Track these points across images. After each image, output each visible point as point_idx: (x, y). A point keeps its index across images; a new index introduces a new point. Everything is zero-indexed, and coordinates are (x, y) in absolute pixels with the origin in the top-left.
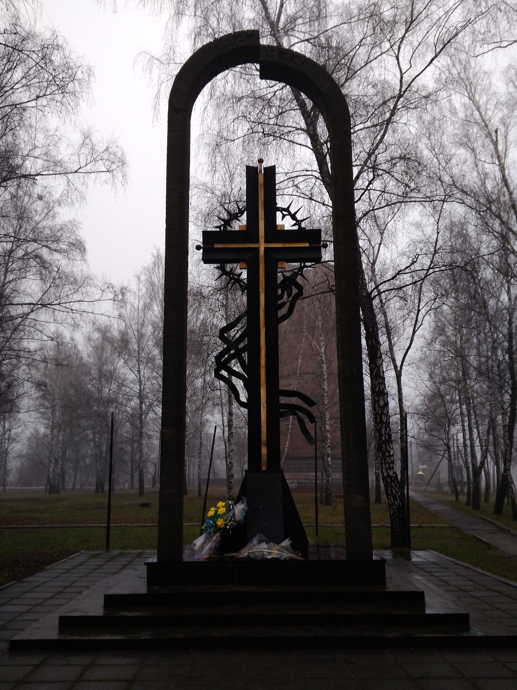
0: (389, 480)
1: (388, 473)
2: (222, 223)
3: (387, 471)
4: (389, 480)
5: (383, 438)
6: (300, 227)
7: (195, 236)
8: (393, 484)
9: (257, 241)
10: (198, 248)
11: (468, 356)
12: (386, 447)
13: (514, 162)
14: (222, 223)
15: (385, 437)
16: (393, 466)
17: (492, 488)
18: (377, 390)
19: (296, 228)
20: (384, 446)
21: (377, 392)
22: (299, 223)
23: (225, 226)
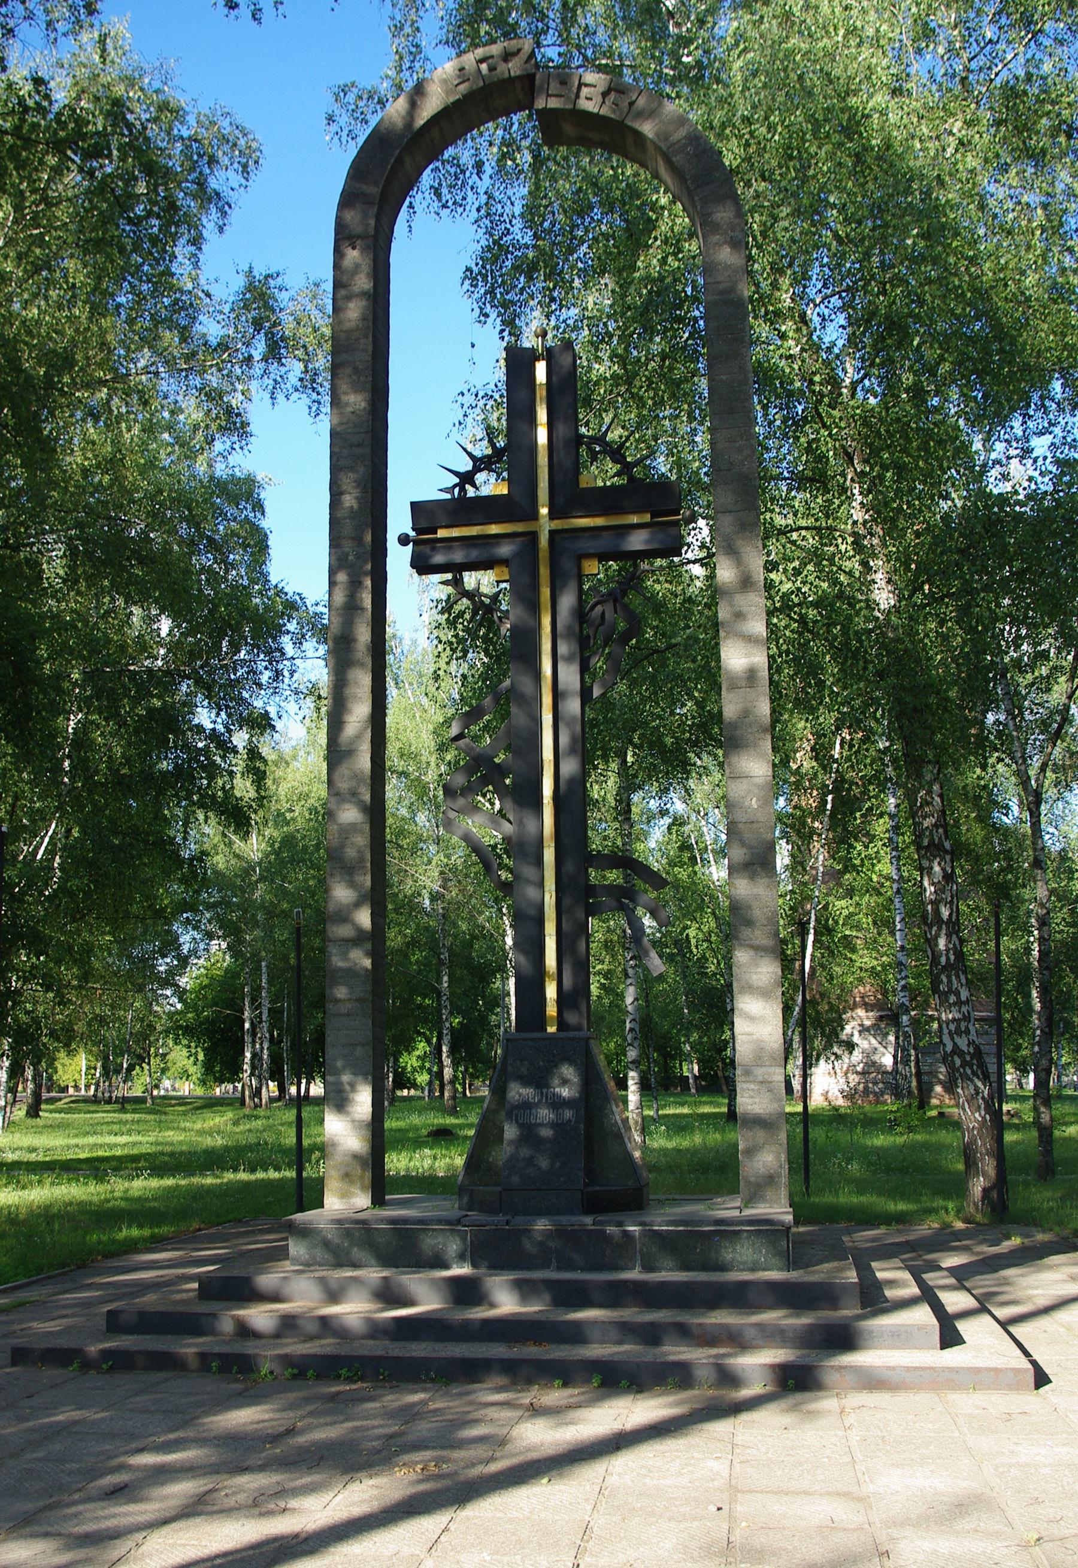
0: (958, 1062)
1: (955, 1044)
2: (457, 480)
3: (952, 1039)
4: (958, 1062)
5: (943, 960)
6: (632, 479)
7: (399, 520)
8: (969, 1071)
9: (535, 516)
10: (404, 540)
11: (202, 856)
12: (950, 981)
13: (1060, 293)
14: (457, 480)
15: (948, 959)
16: (967, 1028)
17: (1034, 994)
18: (926, 842)
19: (622, 481)
20: (945, 980)
21: (927, 848)
22: (626, 468)
23: (461, 486)
